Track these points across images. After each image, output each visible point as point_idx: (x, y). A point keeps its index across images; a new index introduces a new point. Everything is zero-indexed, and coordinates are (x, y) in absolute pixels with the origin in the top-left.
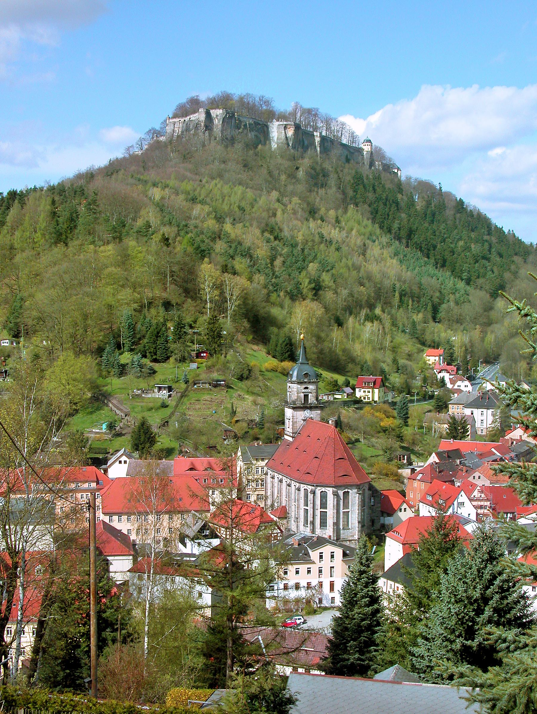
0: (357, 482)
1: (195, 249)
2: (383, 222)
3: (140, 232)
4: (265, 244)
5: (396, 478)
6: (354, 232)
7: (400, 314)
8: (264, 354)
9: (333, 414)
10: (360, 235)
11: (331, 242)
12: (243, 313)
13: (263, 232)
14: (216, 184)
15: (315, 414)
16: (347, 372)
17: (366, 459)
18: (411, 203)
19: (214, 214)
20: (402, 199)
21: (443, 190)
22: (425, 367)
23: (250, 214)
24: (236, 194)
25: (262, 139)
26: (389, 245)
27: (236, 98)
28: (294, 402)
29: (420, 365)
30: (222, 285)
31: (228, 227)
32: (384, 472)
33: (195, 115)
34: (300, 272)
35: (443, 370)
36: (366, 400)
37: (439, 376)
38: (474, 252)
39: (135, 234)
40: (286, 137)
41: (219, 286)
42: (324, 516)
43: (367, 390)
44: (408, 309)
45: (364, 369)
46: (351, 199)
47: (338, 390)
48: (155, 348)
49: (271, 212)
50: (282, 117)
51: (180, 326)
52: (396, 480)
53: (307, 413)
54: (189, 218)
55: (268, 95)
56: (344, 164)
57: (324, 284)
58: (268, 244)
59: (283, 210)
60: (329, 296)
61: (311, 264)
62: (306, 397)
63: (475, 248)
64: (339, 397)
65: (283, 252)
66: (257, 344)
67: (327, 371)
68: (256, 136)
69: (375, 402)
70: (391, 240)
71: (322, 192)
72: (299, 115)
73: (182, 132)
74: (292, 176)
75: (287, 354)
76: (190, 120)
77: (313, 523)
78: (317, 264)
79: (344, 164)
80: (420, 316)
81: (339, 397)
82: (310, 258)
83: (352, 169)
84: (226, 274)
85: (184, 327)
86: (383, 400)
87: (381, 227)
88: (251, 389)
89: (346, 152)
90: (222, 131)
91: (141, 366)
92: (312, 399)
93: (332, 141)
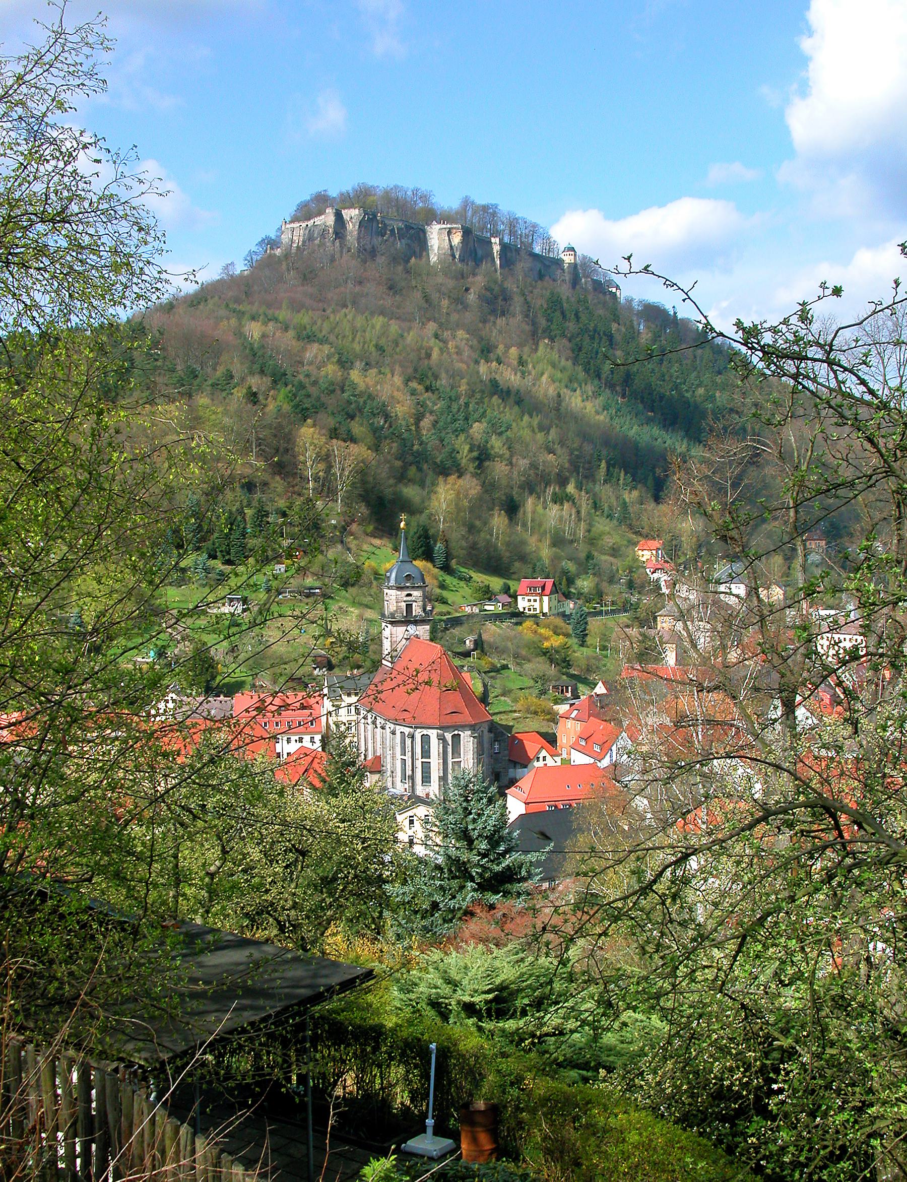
0: (470, 721)
1: (293, 407)
2: (589, 363)
3: (217, 385)
4: (409, 398)
5: (548, 717)
6: (544, 379)
7: (606, 492)
8: (389, 550)
9: (471, 631)
10: (554, 382)
11: (508, 392)
12: (361, 495)
13: (408, 380)
14: (346, 315)
15: (423, 631)
16: (513, 573)
17: (510, 691)
18: (633, 335)
19: (337, 356)
20: (618, 330)
21: (679, 316)
22: (635, 566)
23: (392, 356)
24: (373, 327)
25: (417, 250)
26: (596, 395)
27: (379, 193)
28: (392, 615)
29: (627, 563)
30: (328, 456)
31: (355, 375)
32: (533, 708)
33: (320, 218)
34: (457, 436)
35: (658, 569)
36: (532, 612)
37: (656, 576)
38: (719, 404)
39: (208, 388)
40: (451, 246)
41: (326, 458)
42: (426, 768)
43: (532, 598)
44: (618, 484)
45: (537, 569)
46: (544, 331)
47: (490, 600)
48: (228, 545)
49: (423, 351)
50: (445, 218)
51: (262, 514)
52: (548, 720)
53: (412, 629)
54: (301, 363)
55: (424, 187)
56: (536, 282)
57: (492, 452)
58: (413, 397)
59: (441, 349)
60: (499, 469)
61: (477, 423)
62: (409, 607)
63: (720, 397)
64: (492, 608)
65: (435, 408)
66: (381, 538)
67: (481, 573)
68: (408, 245)
69: (544, 615)
70: (600, 388)
71: (501, 322)
72: (470, 213)
73: (304, 242)
74: (459, 301)
75: (420, 551)
76: (314, 225)
77: (412, 778)
78: (485, 424)
79: (536, 282)
80: (635, 493)
81: (492, 608)
82: (476, 416)
83: (546, 289)
84: (335, 441)
85: (267, 516)
86: (556, 612)
87: (587, 371)
88: (357, 598)
89: (539, 266)
90: (359, 239)
91: (207, 570)
92: (417, 610)
93: (518, 251)
